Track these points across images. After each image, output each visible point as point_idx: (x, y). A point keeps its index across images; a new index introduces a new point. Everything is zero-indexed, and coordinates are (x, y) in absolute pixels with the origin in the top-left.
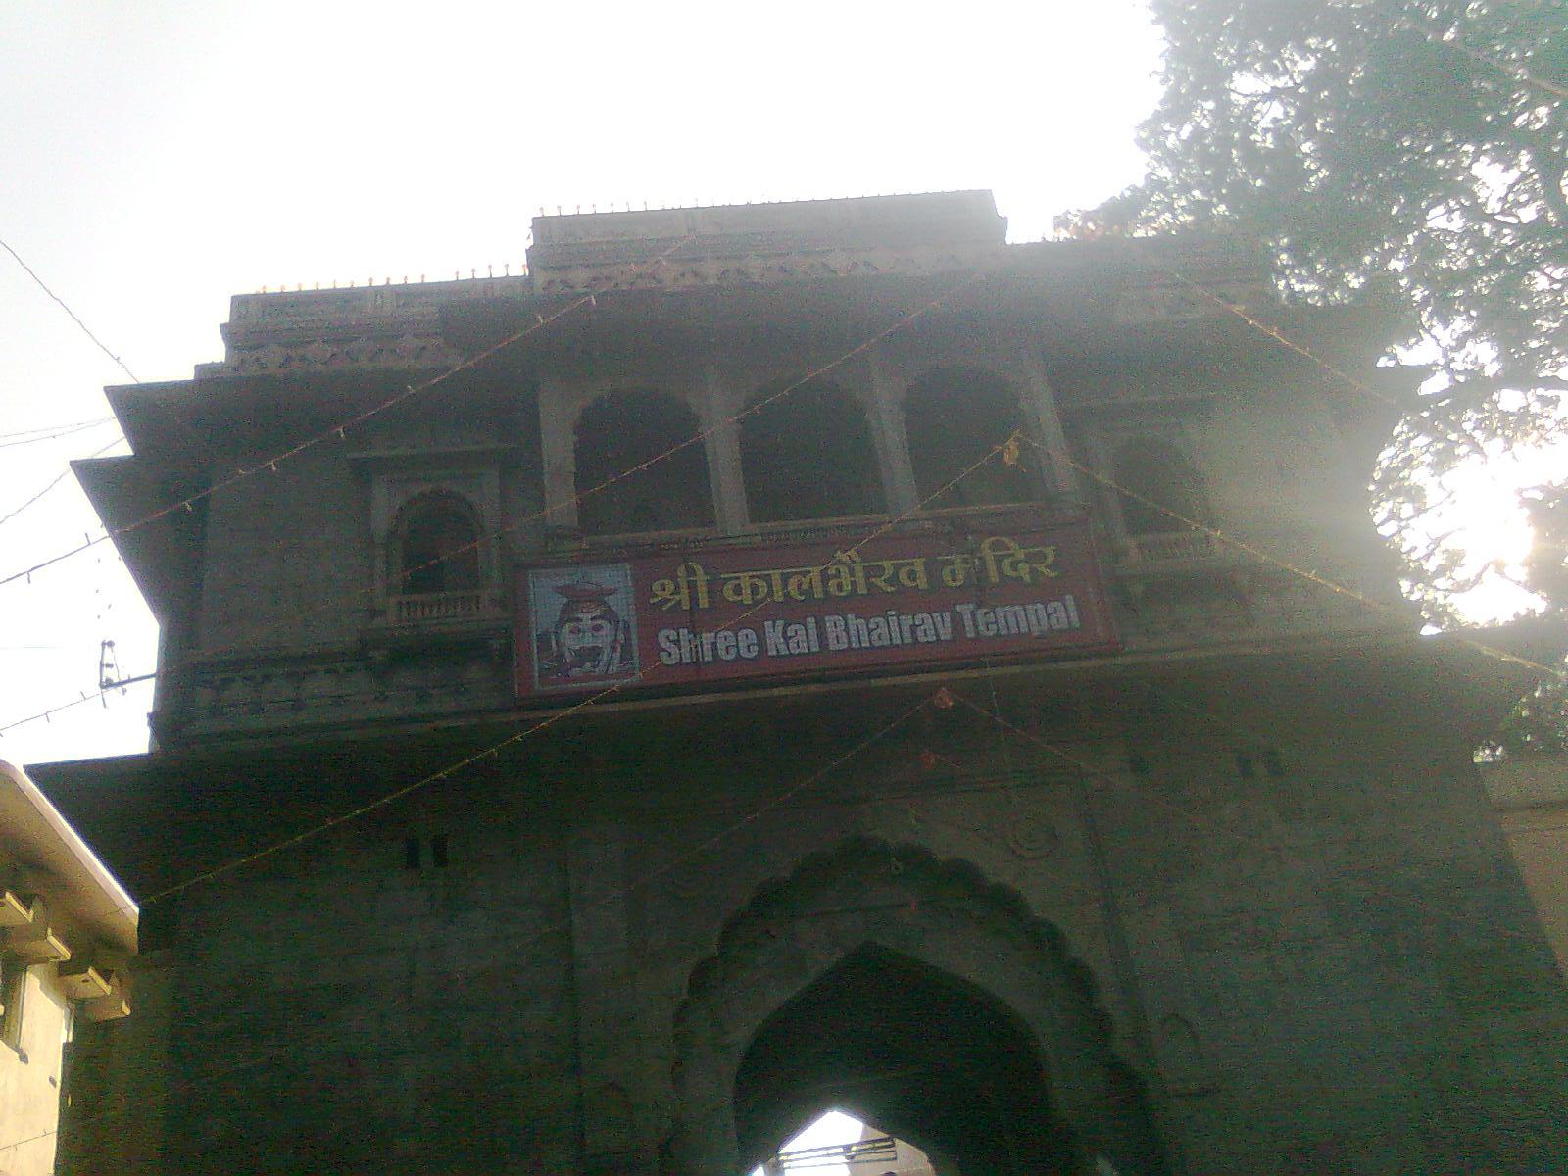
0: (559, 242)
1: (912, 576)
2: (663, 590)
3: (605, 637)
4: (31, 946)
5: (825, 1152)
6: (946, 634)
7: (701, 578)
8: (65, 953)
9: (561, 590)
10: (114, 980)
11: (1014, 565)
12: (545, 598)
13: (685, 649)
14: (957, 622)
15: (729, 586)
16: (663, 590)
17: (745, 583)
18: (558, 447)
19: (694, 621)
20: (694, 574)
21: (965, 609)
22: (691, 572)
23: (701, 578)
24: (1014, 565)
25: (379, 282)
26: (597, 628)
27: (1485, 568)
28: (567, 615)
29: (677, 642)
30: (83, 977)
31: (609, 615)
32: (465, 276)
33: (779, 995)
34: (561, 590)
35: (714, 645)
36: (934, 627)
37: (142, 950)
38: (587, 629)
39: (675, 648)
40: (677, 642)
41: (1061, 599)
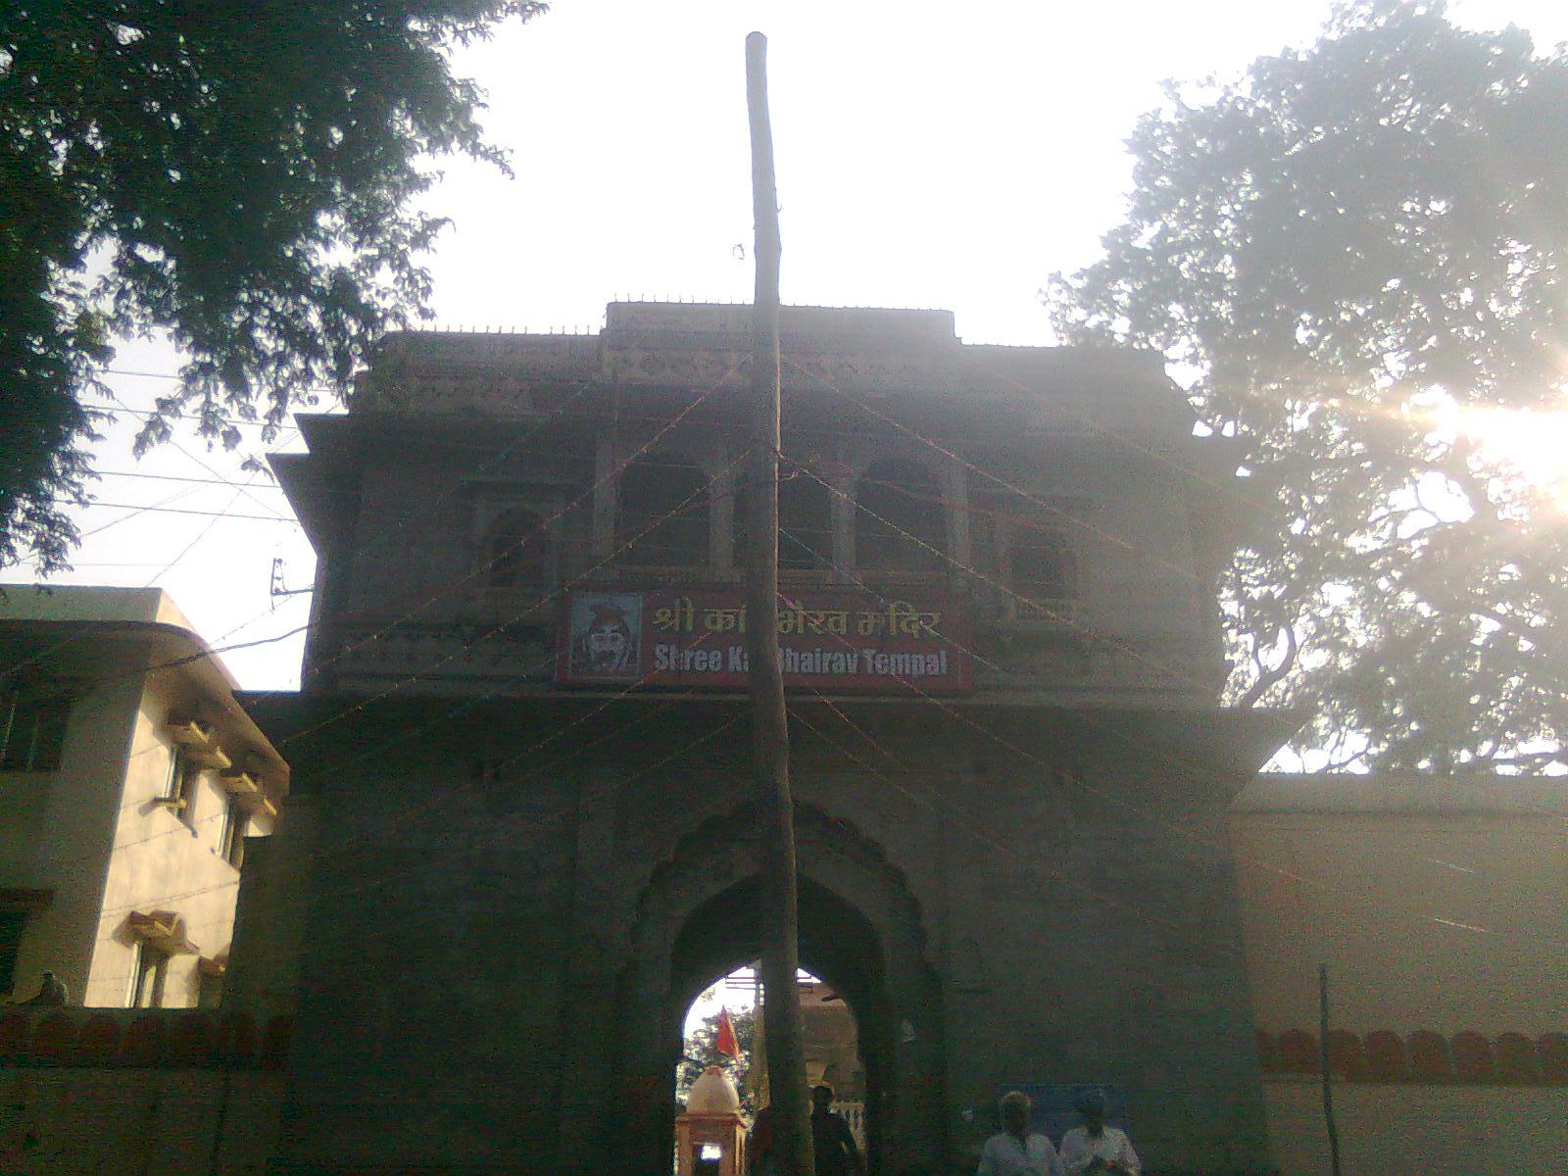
0: (629, 322)
1: (836, 624)
2: (663, 616)
3: (618, 647)
4: (206, 756)
5: (737, 985)
6: (853, 669)
7: (690, 609)
8: (228, 763)
9: (593, 608)
10: (260, 783)
11: (909, 624)
12: (582, 617)
13: (673, 661)
14: (861, 660)
15: (710, 616)
16: (663, 616)
17: (720, 614)
18: (604, 488)
19: (681, 640)
20: (686, 606)
21: (868, 654)
22: (683, 604)
23: (690, 609)
24: (909, 624)
25: (494, 330)
26: (614, 639)
27: (1433, 514)
28: (595, 627)
29: (667, 655)
30: (237, 779)
31: (624, 630)
32: (557, 331)
33: (713, 889)
34: (593, 608)
35: (692, 660)
36: (844, 663)
37: (291, 792)
38: (612, 639)
39: (666, 658)
40: (667, 655)
41: (936, 651)
